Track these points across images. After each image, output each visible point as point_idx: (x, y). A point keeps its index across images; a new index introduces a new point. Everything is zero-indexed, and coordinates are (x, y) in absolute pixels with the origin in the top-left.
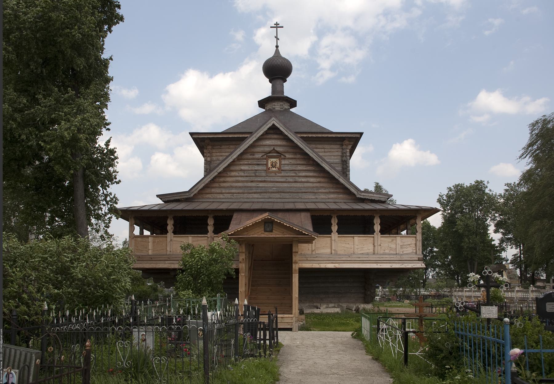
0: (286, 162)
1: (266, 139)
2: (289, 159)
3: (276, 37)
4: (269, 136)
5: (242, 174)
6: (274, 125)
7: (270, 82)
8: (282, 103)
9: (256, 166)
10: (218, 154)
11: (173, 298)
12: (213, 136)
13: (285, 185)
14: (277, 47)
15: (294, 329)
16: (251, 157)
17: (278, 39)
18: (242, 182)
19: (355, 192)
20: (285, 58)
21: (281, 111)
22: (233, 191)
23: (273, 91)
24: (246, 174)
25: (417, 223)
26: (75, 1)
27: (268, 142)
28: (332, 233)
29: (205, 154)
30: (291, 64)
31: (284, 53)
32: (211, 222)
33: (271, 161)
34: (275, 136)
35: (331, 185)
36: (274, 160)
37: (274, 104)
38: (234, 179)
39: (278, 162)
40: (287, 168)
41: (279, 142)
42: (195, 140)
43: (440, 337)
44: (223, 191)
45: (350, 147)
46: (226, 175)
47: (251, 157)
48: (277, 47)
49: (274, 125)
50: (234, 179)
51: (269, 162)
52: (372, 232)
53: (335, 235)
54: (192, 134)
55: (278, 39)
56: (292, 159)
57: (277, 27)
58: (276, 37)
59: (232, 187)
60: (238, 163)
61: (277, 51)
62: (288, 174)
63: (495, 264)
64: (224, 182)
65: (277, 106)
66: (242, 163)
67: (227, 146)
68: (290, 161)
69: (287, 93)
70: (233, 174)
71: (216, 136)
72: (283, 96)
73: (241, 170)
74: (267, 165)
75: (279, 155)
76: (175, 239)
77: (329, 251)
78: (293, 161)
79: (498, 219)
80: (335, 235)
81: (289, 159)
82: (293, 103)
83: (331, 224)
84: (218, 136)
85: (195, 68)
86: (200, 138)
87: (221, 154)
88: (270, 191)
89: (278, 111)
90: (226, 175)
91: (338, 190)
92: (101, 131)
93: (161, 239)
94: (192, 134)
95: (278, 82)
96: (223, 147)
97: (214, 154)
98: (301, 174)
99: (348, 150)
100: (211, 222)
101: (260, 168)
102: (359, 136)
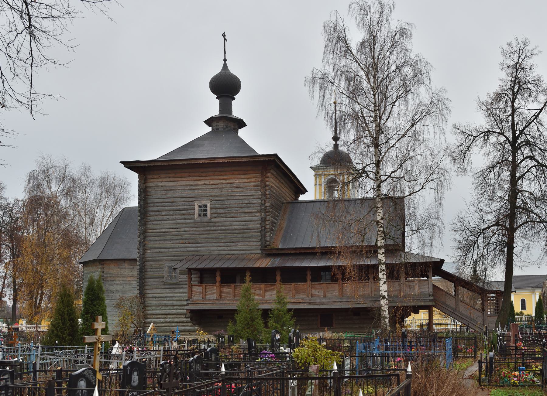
7: (217, 98)
9: (187, 238)
11: (211, 209)
14: (225, 60)
20: (236, 75)
22: (223, 228)
23: (221, 111)
25: (408, 47)
26: (2, 208)
28: (277, 282)
30: (241, 84)
31: (233, 70)
32: (309, 274)
43: (406, 366)
48: (225, 60)
52: (306, 281)
53: (309, 282)
61: (225, 66)
63: (425, 384)
77: (379, 358)
79: (135, 358)
80: (309, 282)
82: (241, 124)
83: (306, 275)
86: (142, 167)
92: (62, 178)
100: (309, 274)
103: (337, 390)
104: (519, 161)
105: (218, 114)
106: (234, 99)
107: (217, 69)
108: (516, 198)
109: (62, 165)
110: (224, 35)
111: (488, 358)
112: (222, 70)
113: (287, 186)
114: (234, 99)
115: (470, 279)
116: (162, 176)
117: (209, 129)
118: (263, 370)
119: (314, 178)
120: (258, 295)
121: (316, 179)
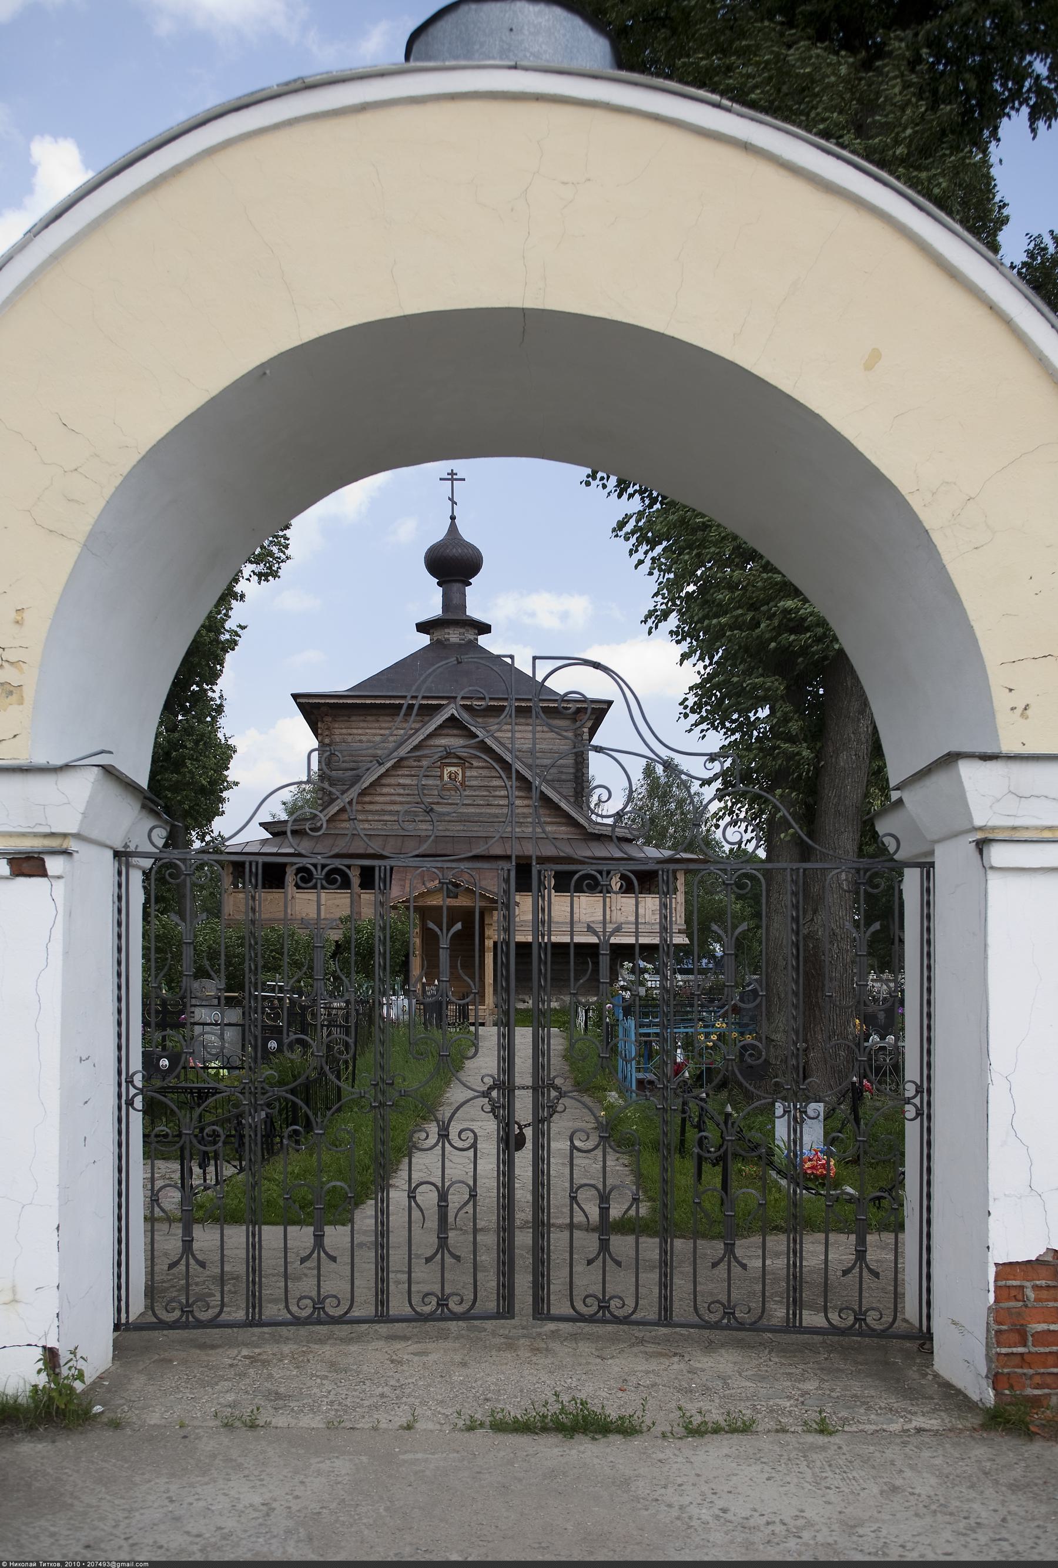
0: (474, 773)
1: (440, 735)
2: (477, 768)
3: (451, 499)
4: (445, 731)
5: (402, 791)
6: (453, 715)
8: (462, 630)
10: (344, 731)
12: (336, 701)
13: (472, 810)
14: (453, 518)
15: (487, 1024)
16: (415, 764)
17: (454, 503)
18: (401, 803)
19: (586, 825)
21: (460, 645)
22: (386, 818)
23: (446, 606)
24: (407, 792)
27: (443, 741)
29: (320, 731)
30: (261, 373)
31: (468, 533)
33: (447, 770)
34: (455, 732)
35: (548, 812)
36: (453, 769)
37: (447, 631)
38: (388, 799)
39: (460, 773)
40: (474, 783)
41: (461, 742)
42: (300, 706)
44: (370, 818)
45: (589, 724)
46: (373, 792)
47: (415, 764)
48: (453, 518)
49: (453, 715)
50: (388, 799)
51: (446, 772)
54: (295, 696)
55: (454, 503)
56: (483, 768)
57: (452, 480)
58: (451, 499)
59: (384, 812)
60: (394, 773)
61: (453, 528)
62: (477, 793)
64: (371, 803)
65: (454, 636)
66: (400, 773)
67: (362, 718)
68: (480, 771)
69: (474, 611)
70: (385, 790)
71: (341, 701)
72: (464, 618)
73: (399, 785)
74: (441, 777)
75: (462, 762)
76: (298, 895)
78: (484, 772)
81: (477, 768)
84: (345, 701)
85: (80, 146)
87: (349, 731)
88: (447, 818)
89: (455, 644)
90: (373, 792)
91: (558, 820)
93: (276, 896)
94: (295, 696)
95: (456, 586)
96: (353, 718)
97: (337, 731)
98: (497, 793)
99: (586, 730)
101: (430, 782)
102: (605, 706)
103: (62, 1414)
104: (289, 1316)
105: (440, 612)
106: (470, 584)
107: (438, 533)
108: (288, 1221)
109: (29, 1388)
110: (954, 1323)
111: (149, 795)
112: (987, 1231)
113: (659, 1349)
114: (470, 584)
115: (716, 740)
116: (369, 718)
117: (425, 640)
118: (798, 1000)
119: (935, 1330)
120: (704, 28)
121: (929, 1328)
